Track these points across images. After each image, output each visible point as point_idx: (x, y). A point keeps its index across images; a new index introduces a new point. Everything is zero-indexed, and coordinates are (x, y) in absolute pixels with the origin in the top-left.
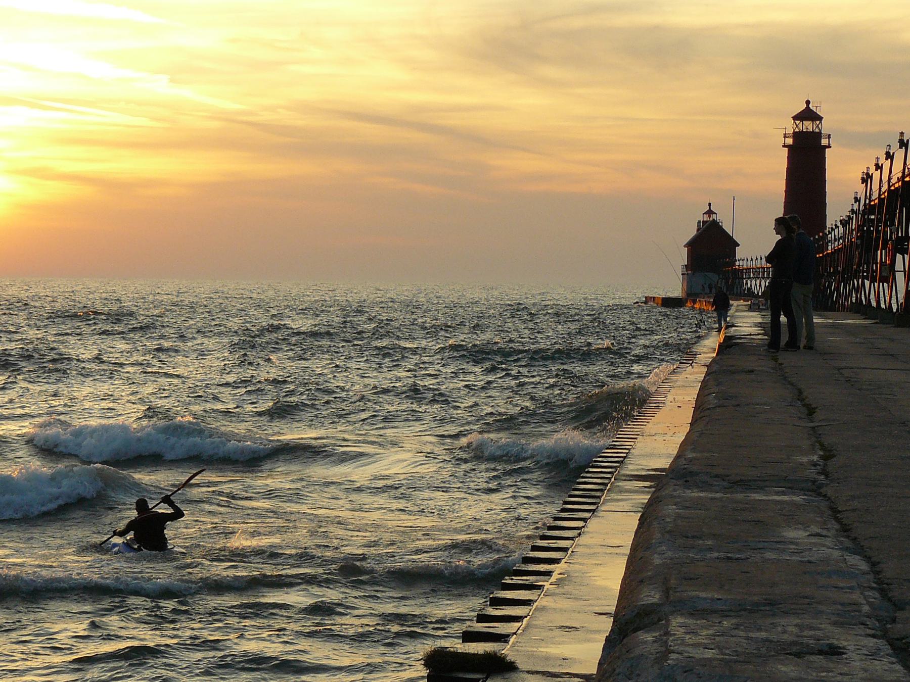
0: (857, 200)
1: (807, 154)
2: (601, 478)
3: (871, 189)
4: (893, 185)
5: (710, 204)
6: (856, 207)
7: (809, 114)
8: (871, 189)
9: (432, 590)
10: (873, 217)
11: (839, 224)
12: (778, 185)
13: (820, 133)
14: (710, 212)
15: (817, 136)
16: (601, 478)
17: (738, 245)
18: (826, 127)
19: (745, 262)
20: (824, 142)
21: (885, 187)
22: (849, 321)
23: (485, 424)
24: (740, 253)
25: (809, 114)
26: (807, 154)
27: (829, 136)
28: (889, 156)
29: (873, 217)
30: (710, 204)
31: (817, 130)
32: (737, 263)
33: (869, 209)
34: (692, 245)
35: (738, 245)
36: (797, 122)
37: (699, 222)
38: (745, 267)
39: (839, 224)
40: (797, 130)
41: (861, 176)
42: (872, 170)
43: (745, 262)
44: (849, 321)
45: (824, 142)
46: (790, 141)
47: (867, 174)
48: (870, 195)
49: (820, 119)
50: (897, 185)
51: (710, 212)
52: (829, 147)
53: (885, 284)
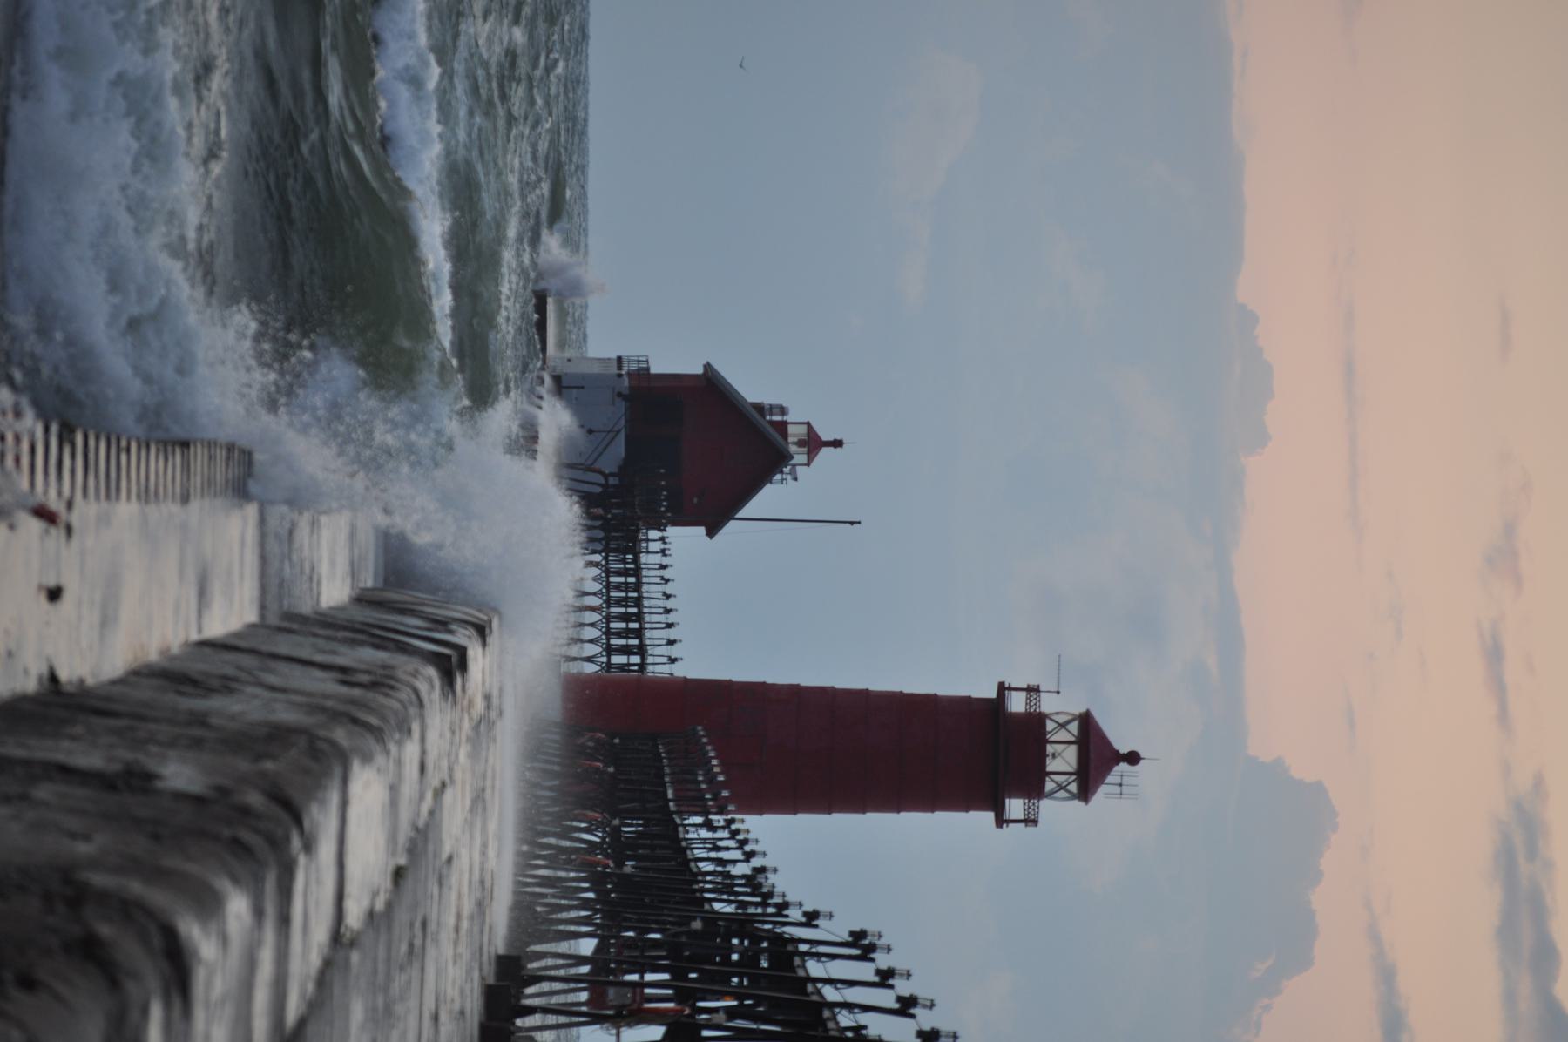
0: (811, 918)
1: (977, 754)
3: (833, 957)
4: (834, 1018)
5: (838, 444)
6: (795, 914)
7: (1098, 758)
8: (833, 957)
9: (462, 1013)
10: (765, 964)
11: (756, 862)
14: (813, 443)
15: (1032, 784)
17: (711, 533)
18: (1057, 810)
19: (658, 559)
20: (1015, 807)
21: (830, 994)
23: (455, 962)
24: (684, 540)
25: (1098, 758)
26: (977, 754)
27: (1031, 821)
28: (906, 1006)
29: (765, 964)
30: (838, 444)
31: (1049, 786)
32: (654, 534)
33: (785, 952)
34: (709, 389)
35: (711, 533)
36: (1074, 727)
37: (783, 410)
38: (644, 558)
39: (756, 862)
40: (1050, 726)
41: (870, 927)
42: (883, 960)
43: (658, 559)
45: (1015, 807)
46: (1017, 703)
47: (872, 948)
48: (818, 956)
49: (1084, 794)
50: (831, 1025)
51: (813, 443)
52: (1001, 821)
53: (584, 996)
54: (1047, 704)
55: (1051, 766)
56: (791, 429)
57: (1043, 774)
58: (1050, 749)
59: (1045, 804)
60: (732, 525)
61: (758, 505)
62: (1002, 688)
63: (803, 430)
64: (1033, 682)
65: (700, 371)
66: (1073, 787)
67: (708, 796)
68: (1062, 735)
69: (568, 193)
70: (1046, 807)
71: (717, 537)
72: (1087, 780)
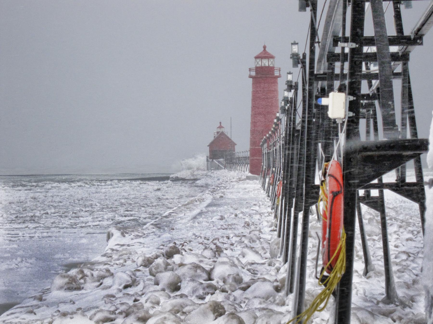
2: (285, 217)
5: (220, 123)
7: (265, 55)
12: (384, 291)
13: (274, 67)
14: (221, 127)
16: (285, 217)
17: (236, 144)
20: (276, 74)
22: (304, 187)
25: (265, 55)
30: (220, 123)
31: (271, 66)
34: (211, 145)
35: (236, 144)
36: (258, 60)
40: (258, 66)
44: (304, 187)
46: (253, 74)
49: (272, 57)
51: (221, 127)
52: (279, 76)
54: (253, 66)
55: (267, 65)
56: (218, 131)
57: (269, 66)
58: (263, 65)
59: (275, 66)
60: (233, 139)
61: (230, 137)
62: (250, 77)
63: (218, 129)
64: (248, 70)
65: (208, 147)
66: (272, 60)
67: (270, 133)
68: (260, 63)
69: (400, 137)
70: (276, 66)
71: (236, 143)
72: (269, 57)
